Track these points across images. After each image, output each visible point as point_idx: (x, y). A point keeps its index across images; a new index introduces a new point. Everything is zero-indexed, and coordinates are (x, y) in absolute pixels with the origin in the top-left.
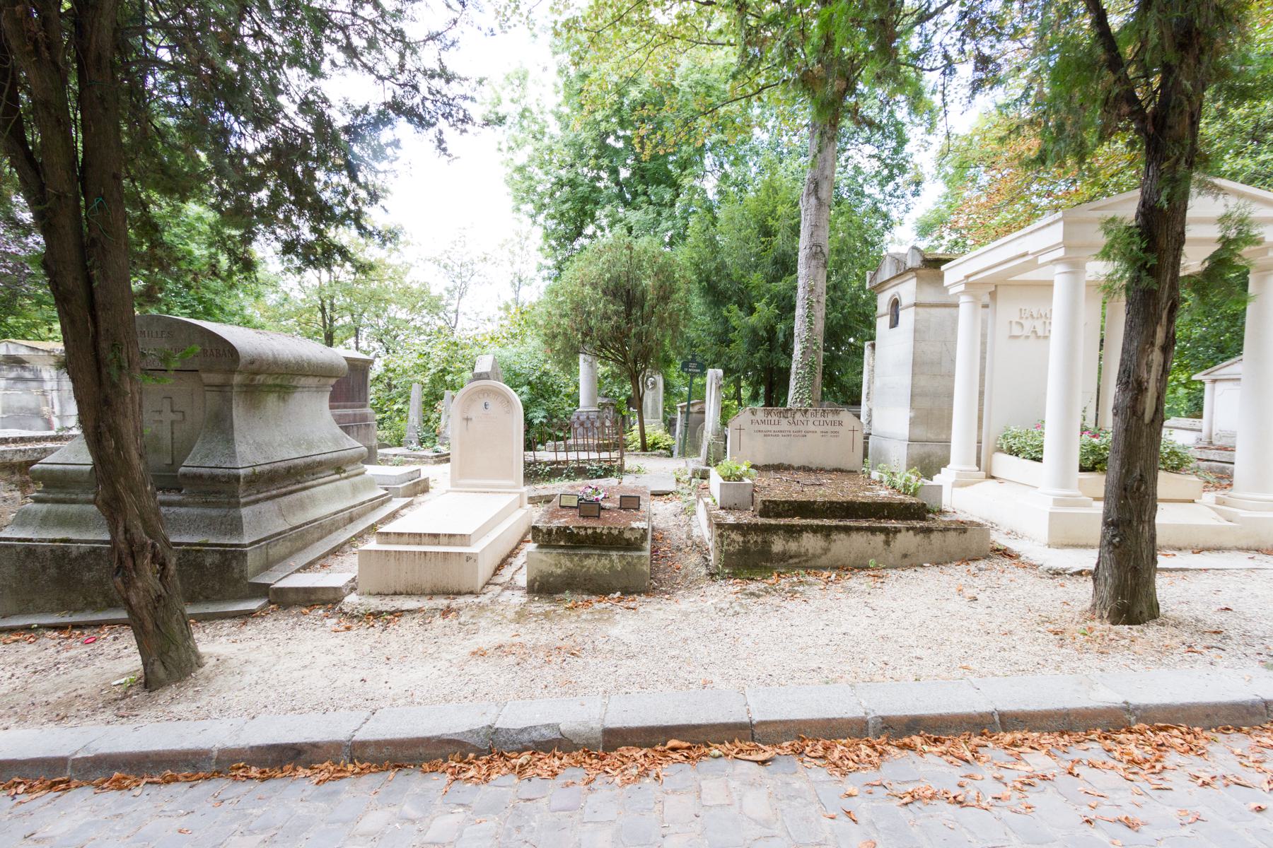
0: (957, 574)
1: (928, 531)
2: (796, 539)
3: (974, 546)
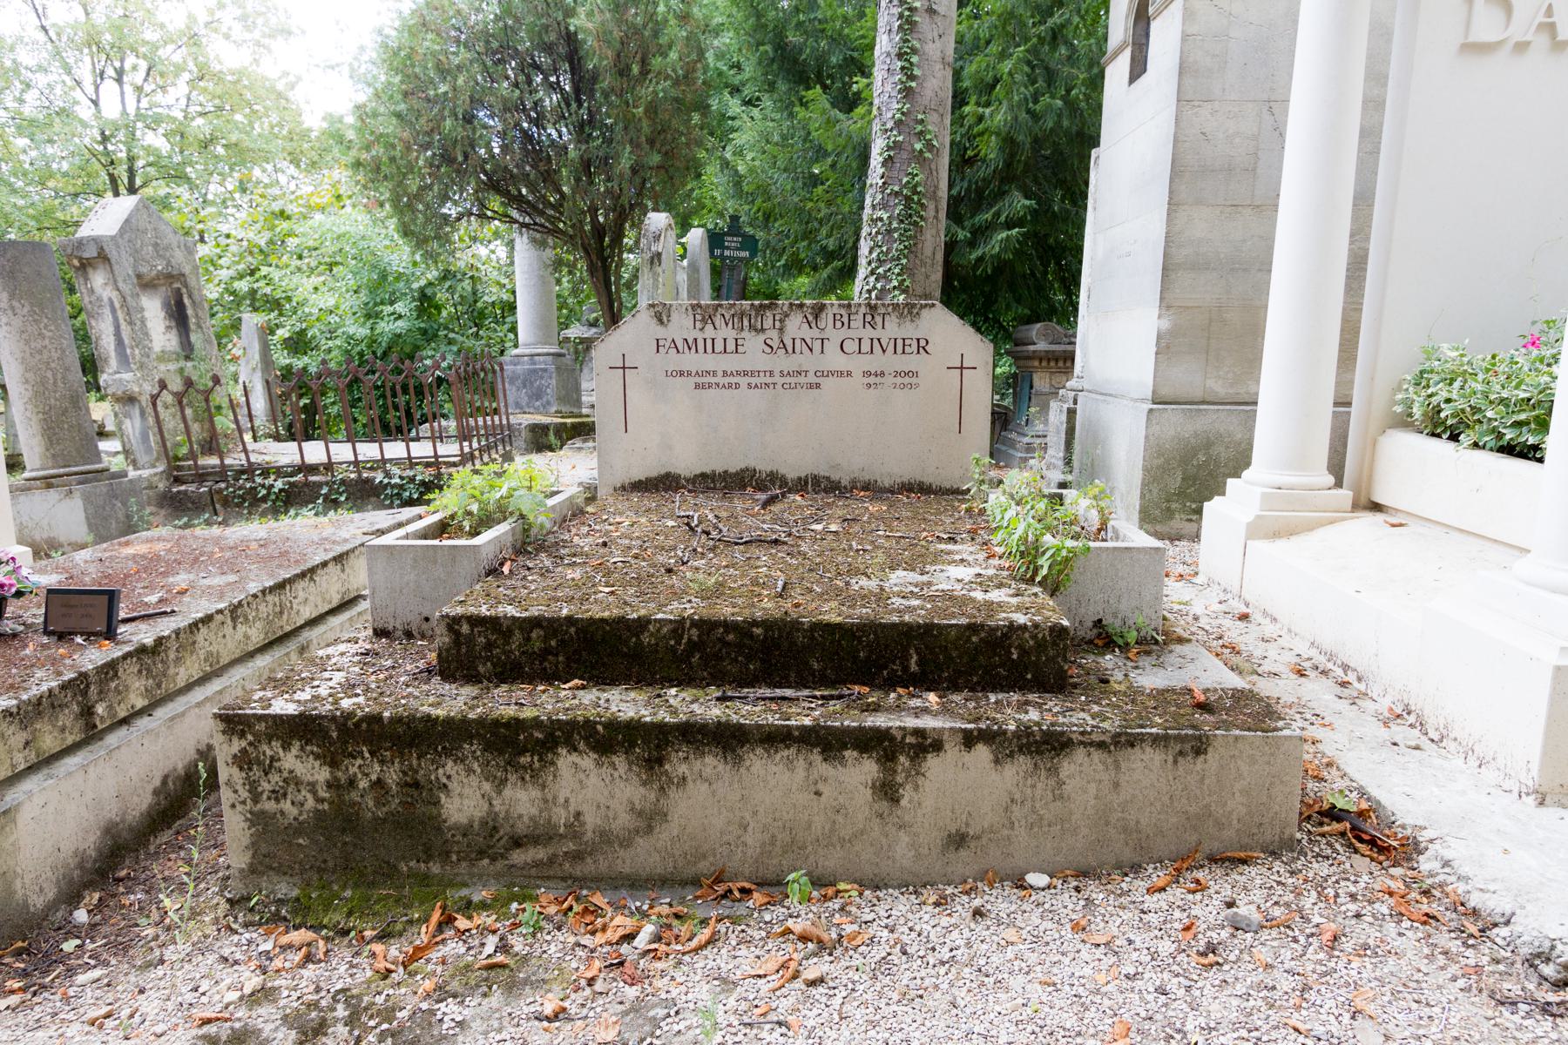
0: (1144, 919)
1: (1049, 746)
2: (533, 776)
3: (1236, 806)
